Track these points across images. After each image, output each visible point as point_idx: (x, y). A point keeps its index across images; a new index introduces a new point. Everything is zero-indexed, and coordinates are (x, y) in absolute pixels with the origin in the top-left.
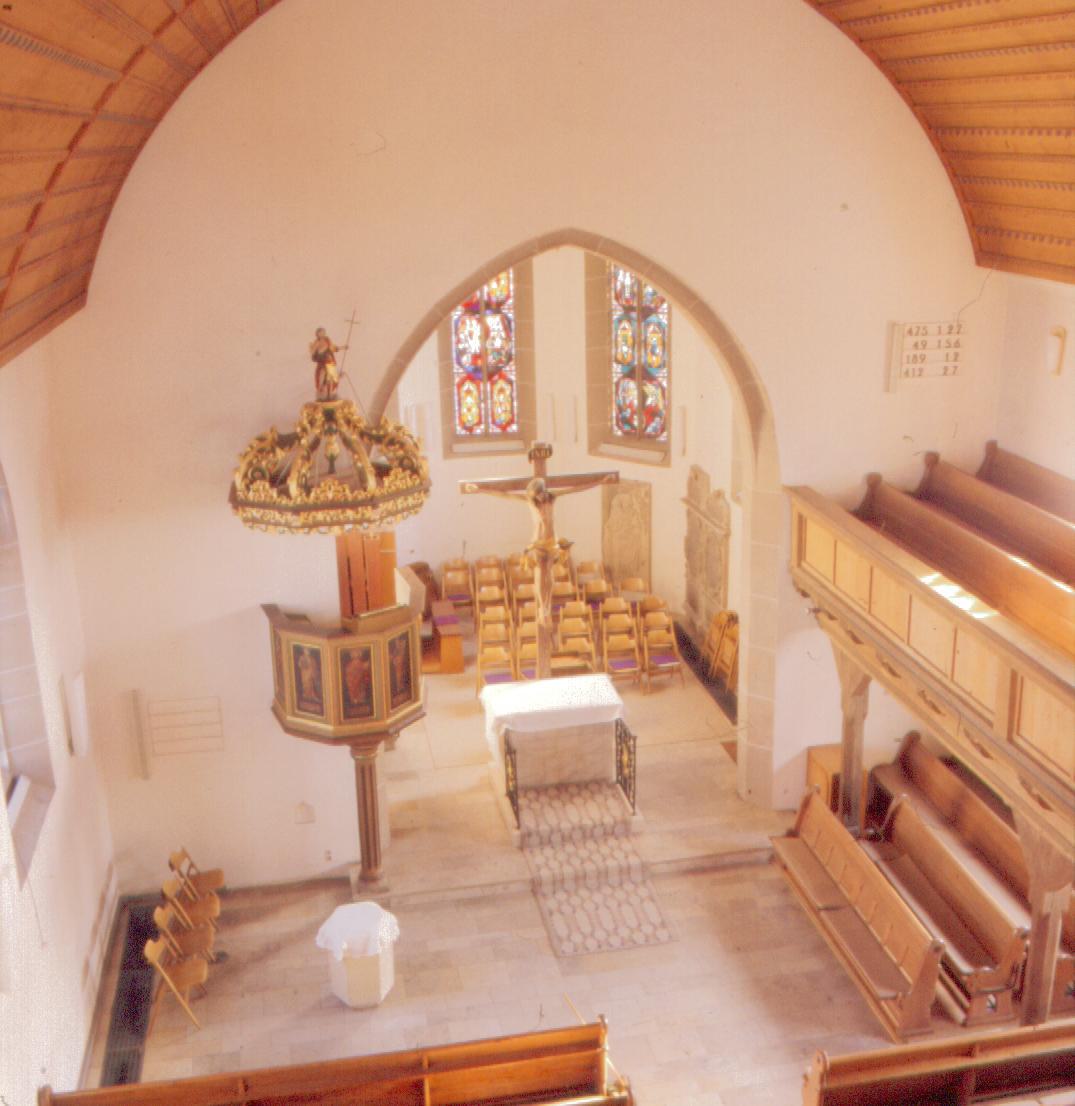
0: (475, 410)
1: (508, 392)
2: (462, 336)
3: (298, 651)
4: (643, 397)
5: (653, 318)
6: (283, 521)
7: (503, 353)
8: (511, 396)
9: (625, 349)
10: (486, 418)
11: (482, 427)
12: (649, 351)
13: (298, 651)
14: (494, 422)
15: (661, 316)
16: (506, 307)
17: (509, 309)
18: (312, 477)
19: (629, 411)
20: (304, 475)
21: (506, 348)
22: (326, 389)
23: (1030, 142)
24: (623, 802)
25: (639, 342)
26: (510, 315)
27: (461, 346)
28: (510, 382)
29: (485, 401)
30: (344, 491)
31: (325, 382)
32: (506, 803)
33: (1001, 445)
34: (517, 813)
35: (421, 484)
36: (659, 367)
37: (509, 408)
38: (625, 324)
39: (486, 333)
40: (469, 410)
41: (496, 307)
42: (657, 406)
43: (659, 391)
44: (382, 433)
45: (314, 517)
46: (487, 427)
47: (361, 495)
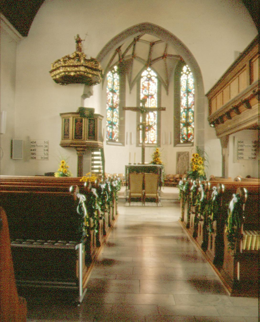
1: (154, 133)
4: (188, 131)
5: (190, 110)
7: (153, 122)
14: (150, 140)
21: (154, 121)
23: (249, 246)
28: (155, 130)
37: (154, 137)
42: (191, 133)
43: (192, 129)
45: (67, 69)
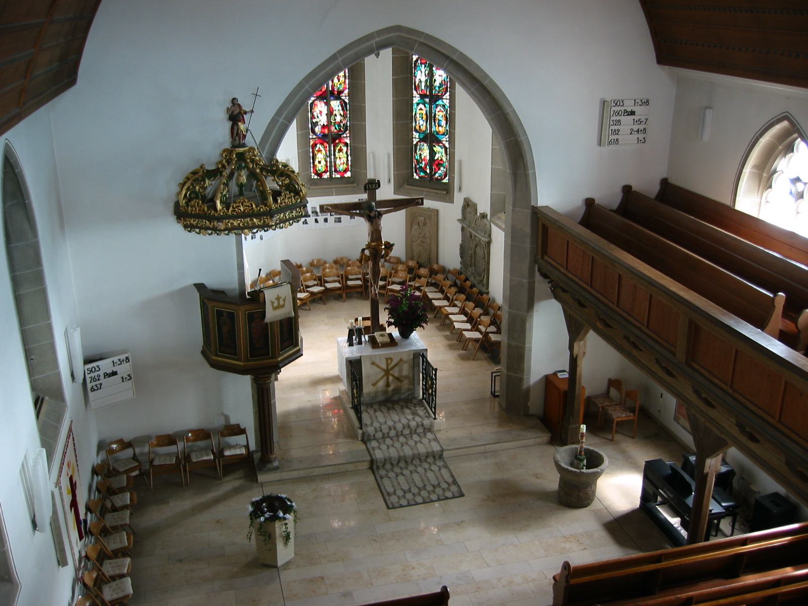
0: (323, 163)
2: (315, 114)
3: (220, 313)
4: (432, 153)
6: (211, 226)
8: (347, 153)
9: (421, 122)
10: (331, 166)
11: (328, 174)
12: (437, 124)
13: (220, 313)
15: (444, 101)
16: (344, 95)
17: (346, 96)
18: (230, 198)
19: (423, 163)
20: (225, 196)
22: (237, 138)
24: (426, 409)
25: (431, 118)
26: (347, 101)
27: (314, 121)
29: (330, 156)
30: (252, 206)
31: (237, 133)
32: (352, 413)
33: (670, 181)
34: (360, 419)
35: (301, 201)
36: (444, 134)
38: (421, 106)
39: (330, 113)
40: (320, 162)
41: (337, 95)
44: (274, 168)
46: (331, 175)
47: (263, 209)
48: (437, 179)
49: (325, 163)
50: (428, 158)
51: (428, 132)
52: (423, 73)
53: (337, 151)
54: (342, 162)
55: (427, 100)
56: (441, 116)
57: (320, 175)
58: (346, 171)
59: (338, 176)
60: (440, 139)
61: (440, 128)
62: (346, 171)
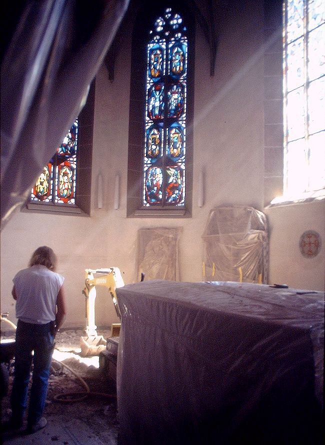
0: (46, 184)
4: (166, 177)
9: (154, 147)
11: (50, 197)
19: (155, 188)
29: (53, 179)
40: (42, 183)
46: (53, 199)
48: (171, 204)
49: (47, 185)
50: (161, 182)
51: (162, 155)
52: (158, 100)
53: (62, 174)
54: (66, 187)
55: (162, 124)
56: (176, 138)
57: (41, 198)
58: (70, 197)
59: (62, 202)
60: (175, 161)
61: (175, 150)
62: (70, 197)
